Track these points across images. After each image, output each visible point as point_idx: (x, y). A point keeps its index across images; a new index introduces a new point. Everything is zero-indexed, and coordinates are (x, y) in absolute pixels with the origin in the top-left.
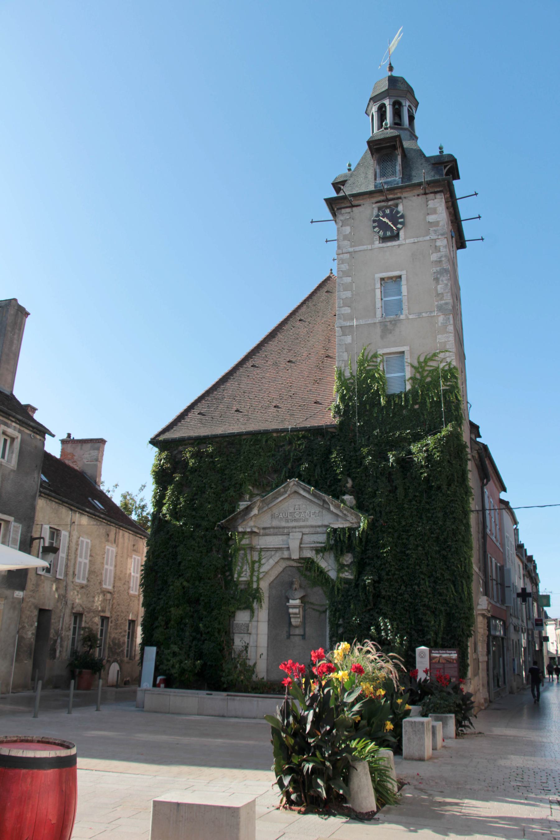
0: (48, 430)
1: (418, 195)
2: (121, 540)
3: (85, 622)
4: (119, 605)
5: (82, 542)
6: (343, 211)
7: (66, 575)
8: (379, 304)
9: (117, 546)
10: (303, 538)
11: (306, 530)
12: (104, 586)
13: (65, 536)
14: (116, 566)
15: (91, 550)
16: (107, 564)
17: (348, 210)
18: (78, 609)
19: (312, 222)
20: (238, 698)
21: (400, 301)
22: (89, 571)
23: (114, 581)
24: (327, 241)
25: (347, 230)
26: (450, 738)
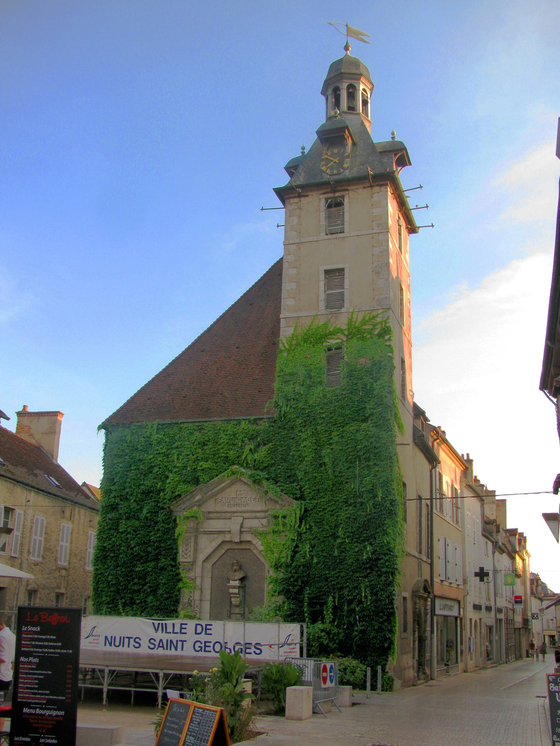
0: (4, 414)
1: (364, 188)
2: (77, 516)
3: (40, 598)
4: (74, 581)
5: (37, 519)
6: (292, 201)
7: (21, 553)
8: (322, 296)
9: (73, 523)
10: (244, 523)
11: (247, 515)
12: (59, 563)
13: (20, 514)
14: (71, 543)
15: (46, 528)
16: (62, 541)
17: (296, 200)
18: (32, 586)
19: (262, 209)
20: (115, 663)
21: (342, 294)
22: (44, 548)
23: (70, 557)
24: (278, 226)
25: (295, 220)
26: (346, 706)
